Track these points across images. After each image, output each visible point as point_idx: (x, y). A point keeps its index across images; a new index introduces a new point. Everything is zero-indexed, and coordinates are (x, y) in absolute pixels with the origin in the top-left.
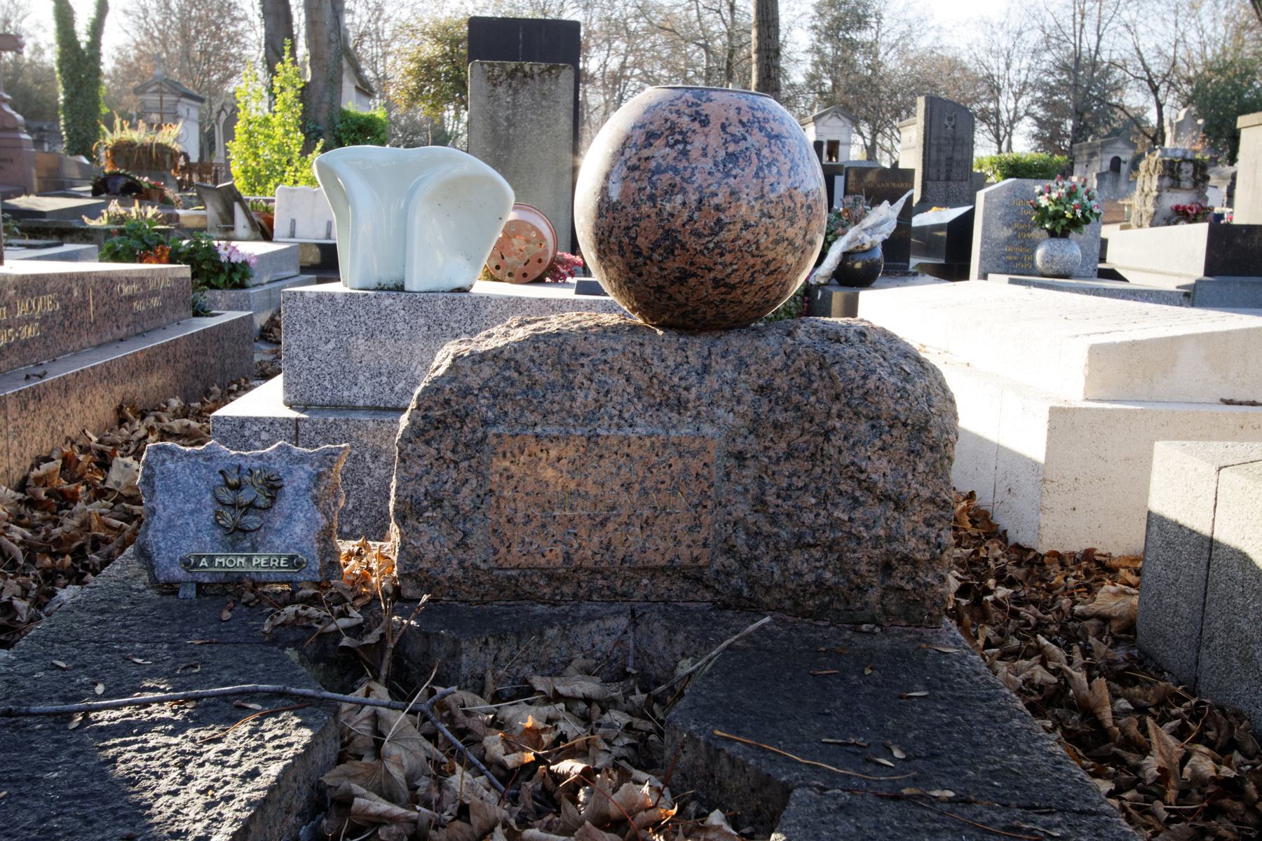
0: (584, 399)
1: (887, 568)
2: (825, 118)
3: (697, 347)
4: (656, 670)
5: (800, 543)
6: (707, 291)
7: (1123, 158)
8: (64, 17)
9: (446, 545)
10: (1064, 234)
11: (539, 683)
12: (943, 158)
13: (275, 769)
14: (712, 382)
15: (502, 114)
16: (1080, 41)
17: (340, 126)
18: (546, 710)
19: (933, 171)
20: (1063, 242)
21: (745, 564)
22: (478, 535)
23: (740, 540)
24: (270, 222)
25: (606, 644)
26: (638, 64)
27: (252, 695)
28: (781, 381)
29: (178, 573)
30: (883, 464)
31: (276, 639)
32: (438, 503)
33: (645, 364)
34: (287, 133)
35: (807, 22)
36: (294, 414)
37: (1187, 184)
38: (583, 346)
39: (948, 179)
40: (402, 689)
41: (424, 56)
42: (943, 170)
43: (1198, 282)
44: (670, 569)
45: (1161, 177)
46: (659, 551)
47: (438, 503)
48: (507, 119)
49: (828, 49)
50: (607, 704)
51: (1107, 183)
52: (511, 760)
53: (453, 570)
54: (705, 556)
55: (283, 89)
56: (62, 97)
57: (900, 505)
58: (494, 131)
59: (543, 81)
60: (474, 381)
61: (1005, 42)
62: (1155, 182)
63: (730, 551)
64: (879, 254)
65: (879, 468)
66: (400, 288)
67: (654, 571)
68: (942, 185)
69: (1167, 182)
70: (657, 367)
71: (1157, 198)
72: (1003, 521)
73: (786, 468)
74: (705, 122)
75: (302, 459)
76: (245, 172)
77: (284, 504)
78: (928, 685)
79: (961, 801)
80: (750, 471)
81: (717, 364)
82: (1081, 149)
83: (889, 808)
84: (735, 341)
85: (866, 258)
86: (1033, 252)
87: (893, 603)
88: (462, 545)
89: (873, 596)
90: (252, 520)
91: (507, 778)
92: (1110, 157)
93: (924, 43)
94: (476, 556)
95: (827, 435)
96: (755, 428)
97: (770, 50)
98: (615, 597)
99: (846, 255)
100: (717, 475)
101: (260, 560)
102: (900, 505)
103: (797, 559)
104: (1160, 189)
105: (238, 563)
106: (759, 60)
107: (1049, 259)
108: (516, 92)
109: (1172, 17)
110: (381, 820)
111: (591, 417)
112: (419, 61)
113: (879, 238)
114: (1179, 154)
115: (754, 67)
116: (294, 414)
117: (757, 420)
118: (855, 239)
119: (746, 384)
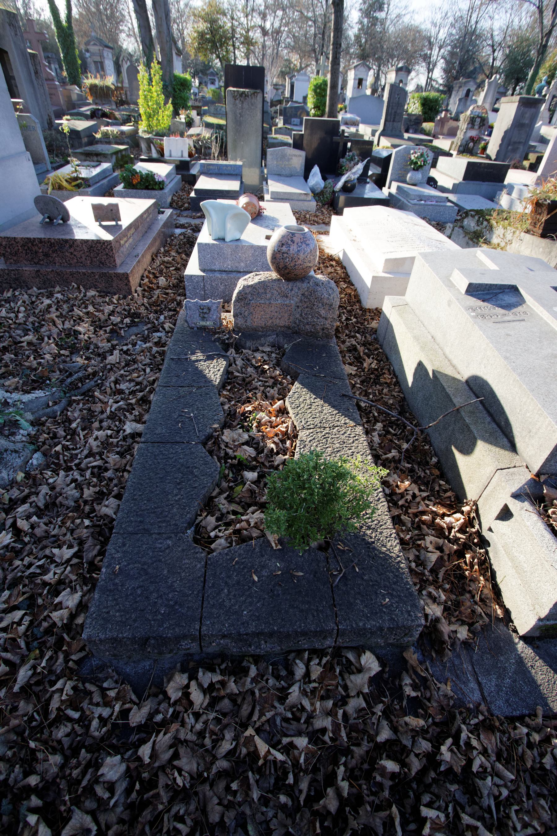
0: (268, 296)
1: (323, 329)
2: (359, 67)
3: (291, 284)
4: (281, 345)
5: (308, 324)
6: (293, 276)
7: (471, 89)
8: (54, 11)
9: (243, 322)
10: (417, 170)
11: (260, 348)
12: (393, 112)
13: (222, 369)
14: (293, 292)
15: (238, 112)
16: (471, 17)
17: (174, 83)
18: (262, 355)
19: (389, 118)
20: (416, 172)
21: (298, 326)
22: (249, 320)
23: (297, 321)
24: (163, 150)
25: (272, 340)
26: (287, 24)
27: (214, 355)
28: (306, 293)
29: (193, 325)
30: (323, 312)
31: (215, 341)
32: (241, 314)
33: (280, 288)
34: (158, 95)
35: (358, 6)
36: (202, 274)
37: (476, 127)
38: (268, 284)
39: (394, 121)
40: (237, 351)
41: (200, 29)
42: (392, 117)
43: (460, 183)
44: (284, 326)
45: (468, 124)
46: (282, 323)
47: (241, 314)
48: (240, 114)
49: (365, 21)
50: (272, 352)
51: (462, 103)
52: (257, 365)
53: (244, 326)
54: (290, 324)
55: (155, 75)
56: (62, 55)
57: (326, 319)
58: (235, 118)
59: (252, 98)
60: (248, 292)
61: (438, 18)
62: (466, 126)
63: (295, 323)
64: (356, 181)
65: (323, 312)
66: (223, 239)
67: (281, 327)
68: (391, 123)
69: (470, 126)
70: (283, 289)
71: (465, 132)
72: (362, 298)
73: (306, 310)
74: (293, 243)
75: (214, 303)
76: (145, 113)
77: (212, 312)
78: (326, 353)
79: (325, 377)
80: (300, 309)
81: (295, 288)
82: (456, 84)
83: (314, 377)
84: (298, 284)
85: (352, 183)
86: (407, 174)
87: (324, 335)
88: (246, 322)
89: (320, 334)
90: (206, 316)
91: (256, 368)
92: (467, 89)
93: (406, 20)
94: (248, 324)
95: (314, 305)
96: (301, 301)
97: (339, 29)
98: (273, 331)
99: (346, 182)
100: (293, 310)
101: (208, 323)
102: (326, 319)
103: (307, 327)
104: (467, 129)
105: (203, 323)
106: (333, 48)
107: (411, 178)
108: (243, 102)
109: (509, 11)
110: (238, 377)
111: (270, 299)
112: (198, 32)
113: (357, 176)
114: (477, 114)
115: (331, 52)
116: (202, 274)
117: (301, 300)
118: (349, 177)
119: (300, 293)
